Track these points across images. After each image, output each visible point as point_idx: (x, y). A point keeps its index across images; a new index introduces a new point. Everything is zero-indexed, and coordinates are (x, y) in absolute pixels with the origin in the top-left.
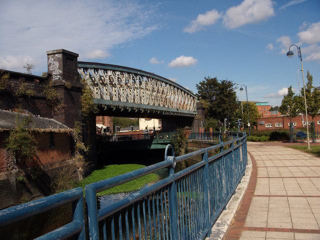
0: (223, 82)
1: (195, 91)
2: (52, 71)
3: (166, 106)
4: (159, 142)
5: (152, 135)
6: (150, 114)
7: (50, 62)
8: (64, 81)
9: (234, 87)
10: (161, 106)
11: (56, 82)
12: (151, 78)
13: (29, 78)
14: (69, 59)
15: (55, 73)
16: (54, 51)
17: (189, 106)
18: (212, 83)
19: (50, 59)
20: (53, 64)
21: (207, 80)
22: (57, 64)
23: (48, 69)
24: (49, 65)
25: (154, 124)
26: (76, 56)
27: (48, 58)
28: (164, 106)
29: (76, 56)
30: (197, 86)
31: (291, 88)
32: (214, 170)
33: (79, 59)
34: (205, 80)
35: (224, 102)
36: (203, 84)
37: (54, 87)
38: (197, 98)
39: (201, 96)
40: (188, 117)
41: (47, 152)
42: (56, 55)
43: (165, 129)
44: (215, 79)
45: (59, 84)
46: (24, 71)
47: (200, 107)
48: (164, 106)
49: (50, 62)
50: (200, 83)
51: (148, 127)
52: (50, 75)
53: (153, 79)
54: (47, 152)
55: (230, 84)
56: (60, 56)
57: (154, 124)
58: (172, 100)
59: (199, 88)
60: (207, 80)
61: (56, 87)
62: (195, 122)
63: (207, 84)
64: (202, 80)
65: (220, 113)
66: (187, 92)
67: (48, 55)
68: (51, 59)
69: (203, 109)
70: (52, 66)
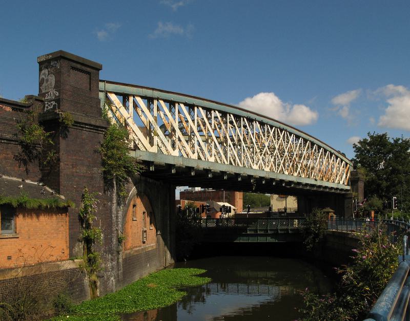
0: (396, 141)
1: (351, 155)
15: (49, 97)
16: (48, 55)
17: (339, 180)
19: (43, 72)
21: (372, 137)
23: (40, 89)
25: (291, 203)
27: (40, 70)
30: (355, 146)
31: (27, 174)
32: (111, 200)
36: (364, 142)
39: (360, 162)
40: (339, 194)
41: (31, 215)
44: (383, 135)
51: (288, 206)
54: (31, 215)
57: (291, 203)
59: (358, 150)
70: (45, 84)
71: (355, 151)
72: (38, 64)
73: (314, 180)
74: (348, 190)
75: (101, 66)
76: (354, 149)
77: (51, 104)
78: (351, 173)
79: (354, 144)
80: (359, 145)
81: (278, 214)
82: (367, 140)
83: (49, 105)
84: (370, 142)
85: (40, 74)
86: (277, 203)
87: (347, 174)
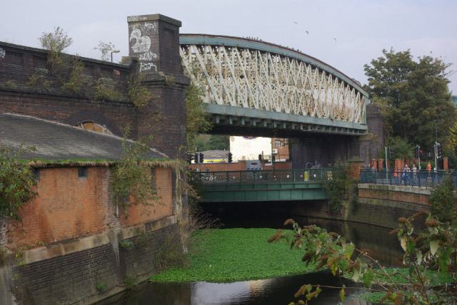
1: (364, 80)
2: (139, 54)
3: (313, 115)
4: (296, 186)
5: (262, 171)
6: (251, 128)
7: (133, 36)
8: (162, 74)
9: (446, 71)
10: (305, 114)
11: (148, 74)
12: (295, 59)
13: (107, 67)
14: (167, 28)
15: (144, 58)
16: (142, 16)
18: (399, 63)
19: (134, 32)
20: (140, 41)
21: (388, 56)
22: (147, 41)
24: (132, 43)
26: (178, 24)
27: (130, 30)
28: (309, 114)
29: (178, 24)
30: (367, 68)
33: (182, 30)
34: (385, 57)
35: (425, 104)
36: (378, 64)
37: (143, 83)
38: (367, 95)
42: (146, 25)
43: (295, 163)
45: (152, 79)
46: (97, 56)
47: (371, 115)
48: (309, 114)
49: (133, 36)
50: (374, 63)
52: (134, 62)
53: (299, 61)
55: (438, 67)
56: (154, 26)
58: (322, 100)
59: (371, 73)
60: (388, 56)
61: (151, 83)
62: (364, 146)
63: (387, 66)
64: (377, 55)
65: (415, 127)
66: (346, 83)
67: (130, 23)
68: (136, 31)
69: (378, 116)
71: (366, 74)
72: (127, 24)
73: (329, 120)
74: (364, 131)
75: (181, 23)
76: (365, 70)
77: (149, 66)
78: (367, 107)
79: (366, 65)
80: (373, 67)
81: (259, 163)
82: (384, 60)
83: (145, 66)
84: (387, 63)
85: (130, 34)
86: (247, 149)
87: (362, 108)
